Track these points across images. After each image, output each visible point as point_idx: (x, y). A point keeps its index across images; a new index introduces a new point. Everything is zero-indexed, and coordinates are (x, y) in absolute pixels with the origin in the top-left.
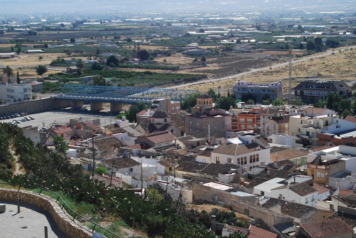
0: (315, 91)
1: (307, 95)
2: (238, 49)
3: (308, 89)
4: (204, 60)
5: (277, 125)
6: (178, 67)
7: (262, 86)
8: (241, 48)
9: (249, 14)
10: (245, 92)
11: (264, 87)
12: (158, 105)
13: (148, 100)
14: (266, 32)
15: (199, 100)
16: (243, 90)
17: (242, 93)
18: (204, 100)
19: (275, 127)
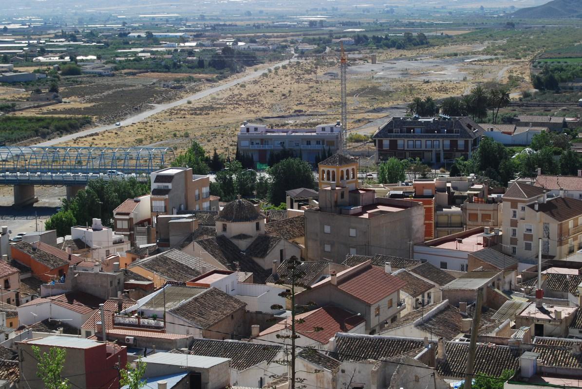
0: (423, 140)
1: (406, 148)
2: (88, 70)
3: (407, 137)
4: (54, 89)
5: (554, 225)
6: (14, 105)
7: (297, 134)
8: (93, 69)
9: (20, 19)
10: (267, 147)
11: (302, 134)
12: (170, 185)
13: (91, 174)
14: (94, 44)
15: (326, 169)
16: (262, 144)
17: (260, 151)
18: (341, 170)
19: (546, 229)
